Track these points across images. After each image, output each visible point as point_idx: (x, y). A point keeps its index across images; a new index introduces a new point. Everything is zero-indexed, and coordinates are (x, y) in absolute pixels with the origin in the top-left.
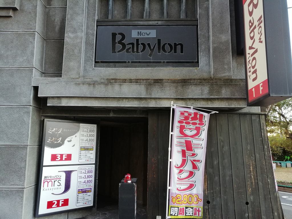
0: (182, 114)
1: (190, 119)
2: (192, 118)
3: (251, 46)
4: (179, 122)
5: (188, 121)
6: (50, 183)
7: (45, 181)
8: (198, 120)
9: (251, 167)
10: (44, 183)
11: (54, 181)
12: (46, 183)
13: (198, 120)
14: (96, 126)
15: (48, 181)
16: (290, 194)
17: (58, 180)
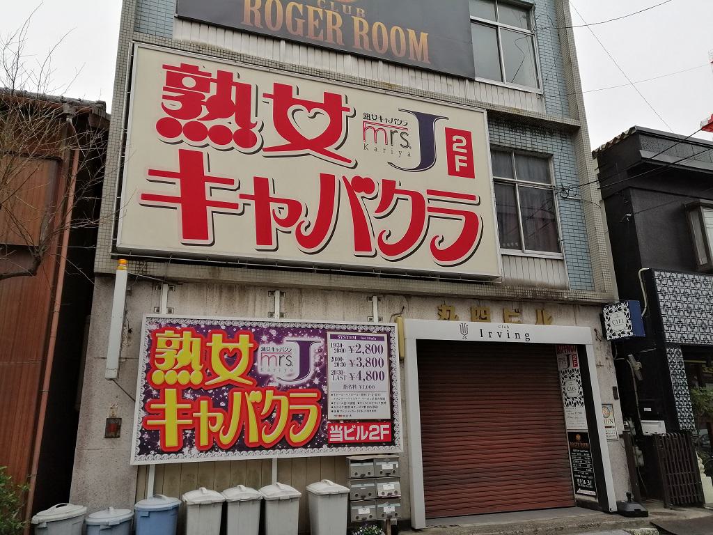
0: (173, 79)
1: (205, 112)
2: (209, 104)
3: (397, 187)
4: (167, 128)
5: (195, 120)
6: (273, 360)
7: (263, 355)
8: (233, 118)
9: (636, 393)
10: (262, 358)
11: (280, 357)
12: (265, 359)
13: (233, 118)
14: (663, 422)
15: (269, 355)
16: (126, 80)
17: (286, 356)
